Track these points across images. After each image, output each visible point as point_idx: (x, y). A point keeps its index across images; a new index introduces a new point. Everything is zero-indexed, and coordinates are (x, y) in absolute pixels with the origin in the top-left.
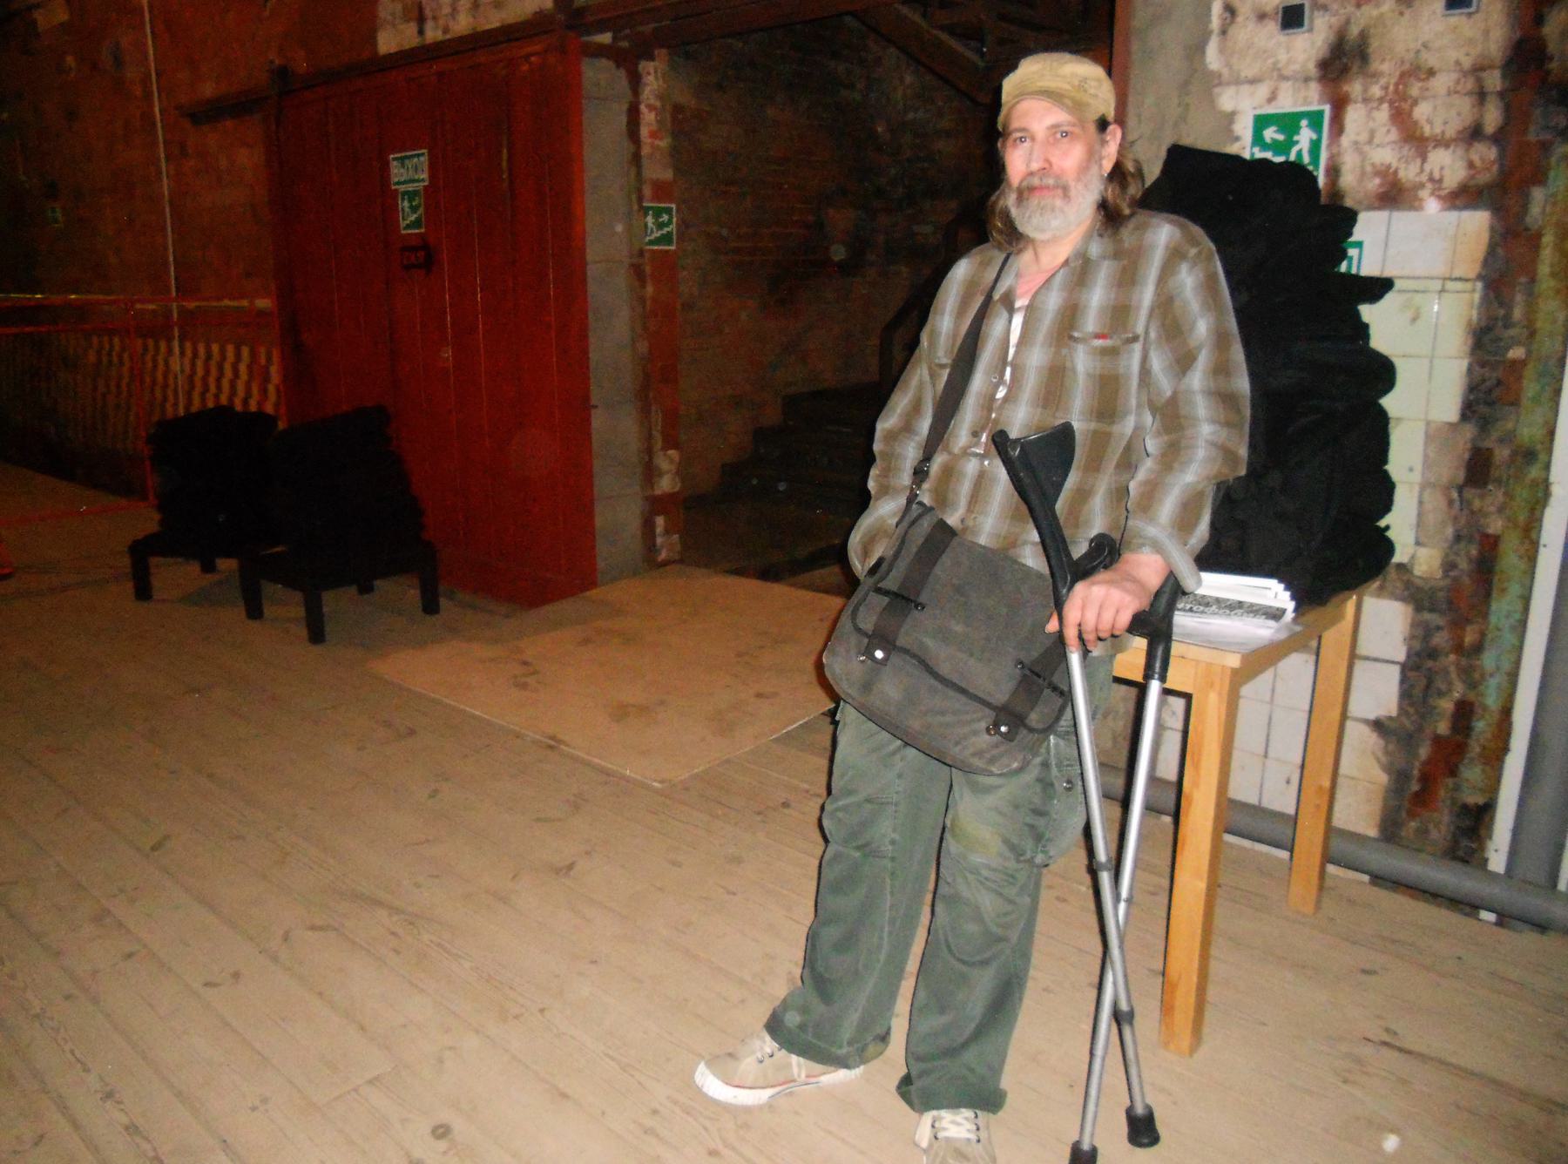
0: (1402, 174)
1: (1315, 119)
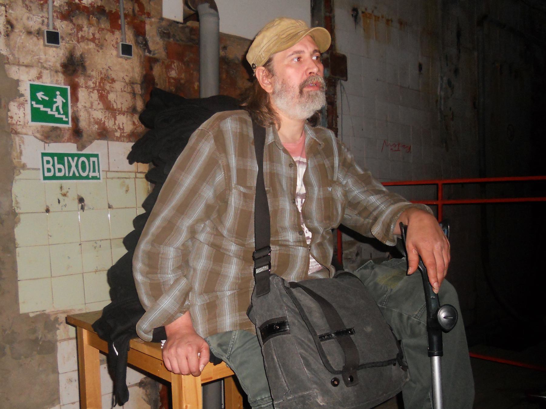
0: (106, 124)
1: (64, 93)
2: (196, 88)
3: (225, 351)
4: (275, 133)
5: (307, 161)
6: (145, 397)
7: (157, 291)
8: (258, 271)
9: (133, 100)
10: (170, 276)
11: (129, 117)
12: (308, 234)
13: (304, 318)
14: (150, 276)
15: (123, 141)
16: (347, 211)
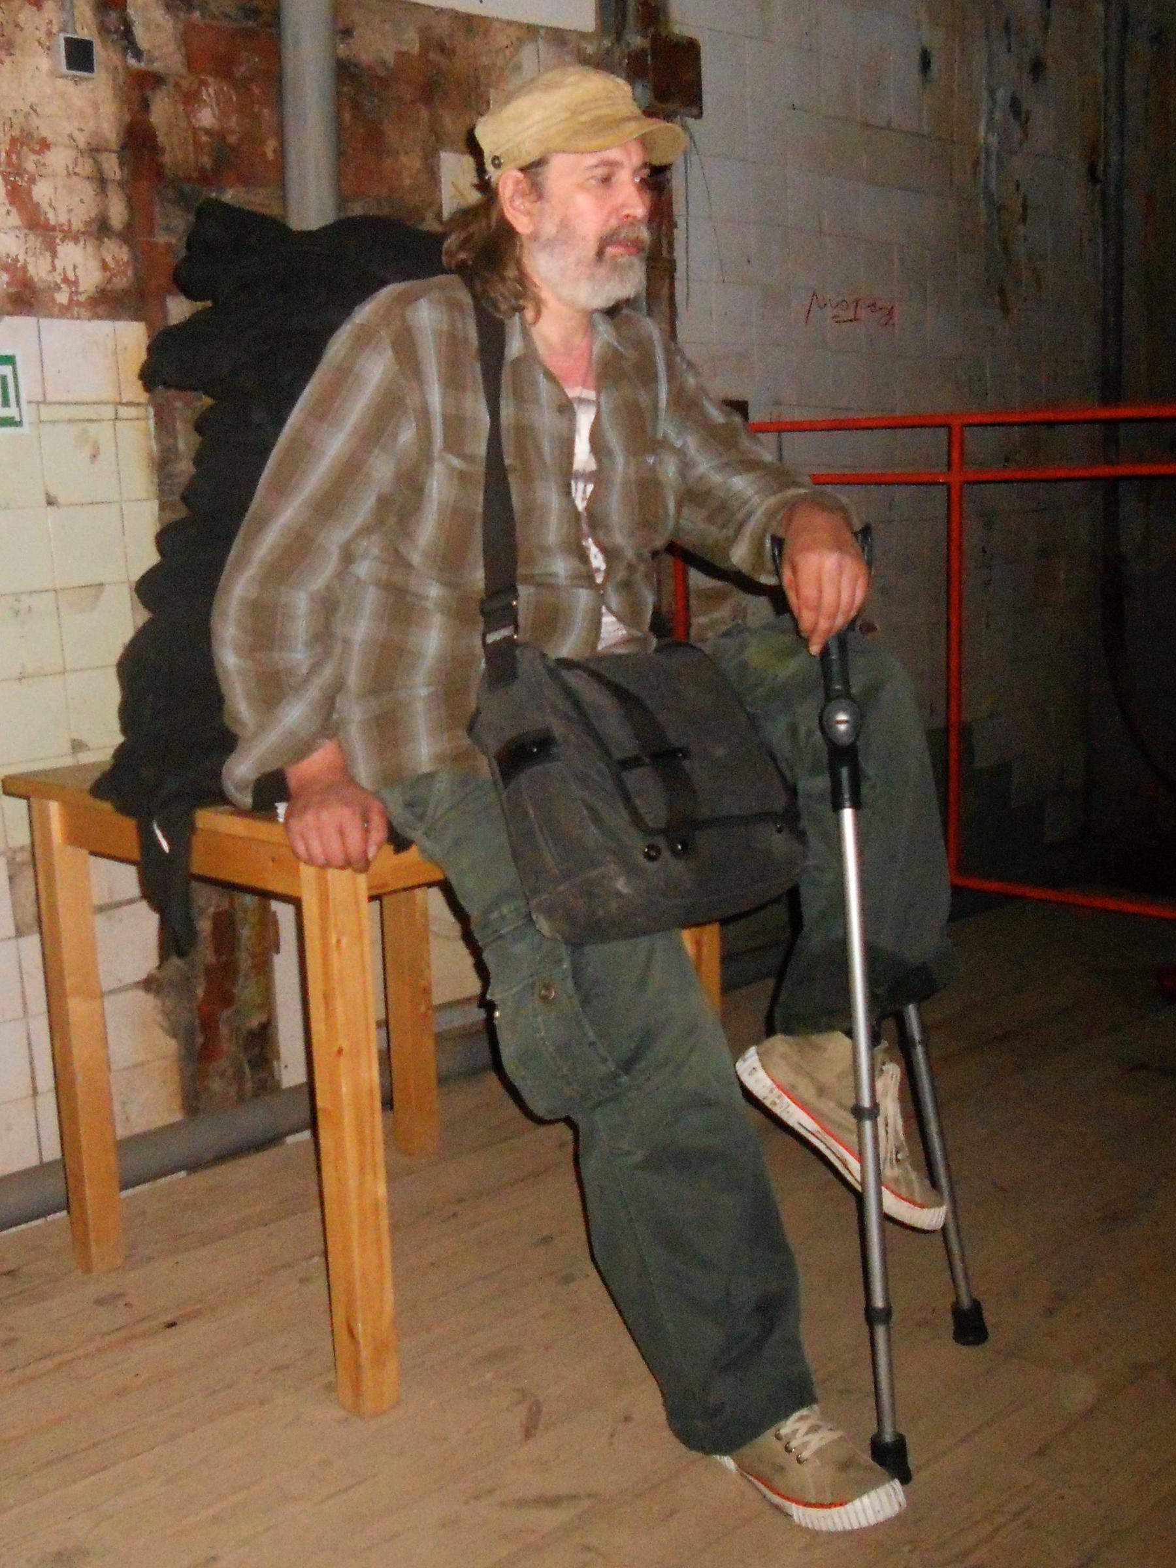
0: (31, 270)
2: (270, 155)
3: (421, 818)
4: (526, 334)
5: (598, 393)
6: (159, 1018)
7: (273, 689)
8: (491, 638)
9: (98, 198)
10: (299, 656)
11: (90, 249)
12: (597, 560)
13: (589, 728)
14: (258, 655)
15: (78, 318)
16: (685, 511)
